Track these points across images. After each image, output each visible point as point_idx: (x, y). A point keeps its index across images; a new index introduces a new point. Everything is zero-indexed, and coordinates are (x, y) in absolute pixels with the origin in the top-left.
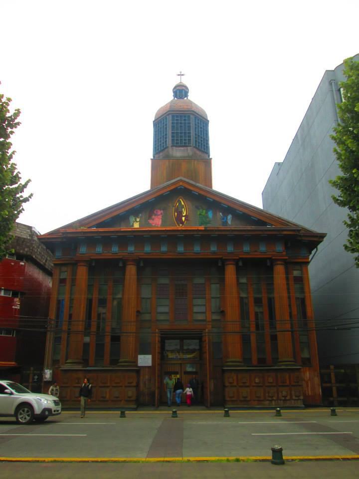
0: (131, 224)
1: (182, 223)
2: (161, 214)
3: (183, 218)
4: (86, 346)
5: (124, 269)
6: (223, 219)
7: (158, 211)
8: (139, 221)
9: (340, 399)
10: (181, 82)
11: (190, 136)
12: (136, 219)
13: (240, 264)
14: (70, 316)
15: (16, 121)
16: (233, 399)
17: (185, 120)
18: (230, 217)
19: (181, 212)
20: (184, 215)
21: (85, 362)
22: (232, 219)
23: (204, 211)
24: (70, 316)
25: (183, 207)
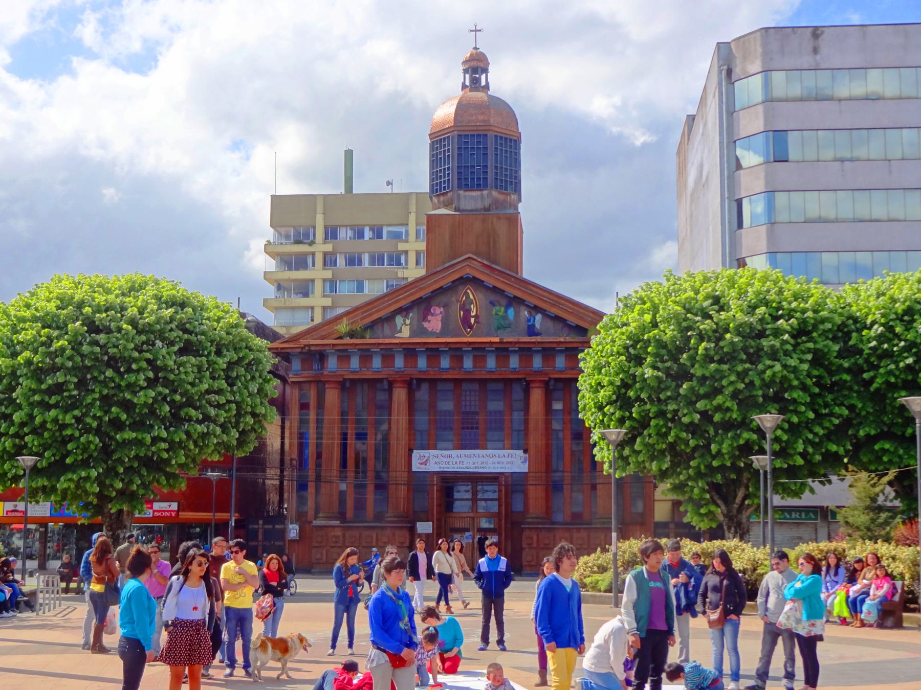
0: (399, 328)
1: (471, 327)
2: (441, 313)
3: (472, 320)
4: (342, 494)
5: (390, 390)
6: (529, 320)
7: (437, 308)
9: (823, 573)
10: (476, 48)
12: (404, 321)
14: (319, 456)
16: (532, 563)
19: (469, 311)
20: (473, 314)
21: (342, 516)
23: (503, 309)
24: (319, 456)
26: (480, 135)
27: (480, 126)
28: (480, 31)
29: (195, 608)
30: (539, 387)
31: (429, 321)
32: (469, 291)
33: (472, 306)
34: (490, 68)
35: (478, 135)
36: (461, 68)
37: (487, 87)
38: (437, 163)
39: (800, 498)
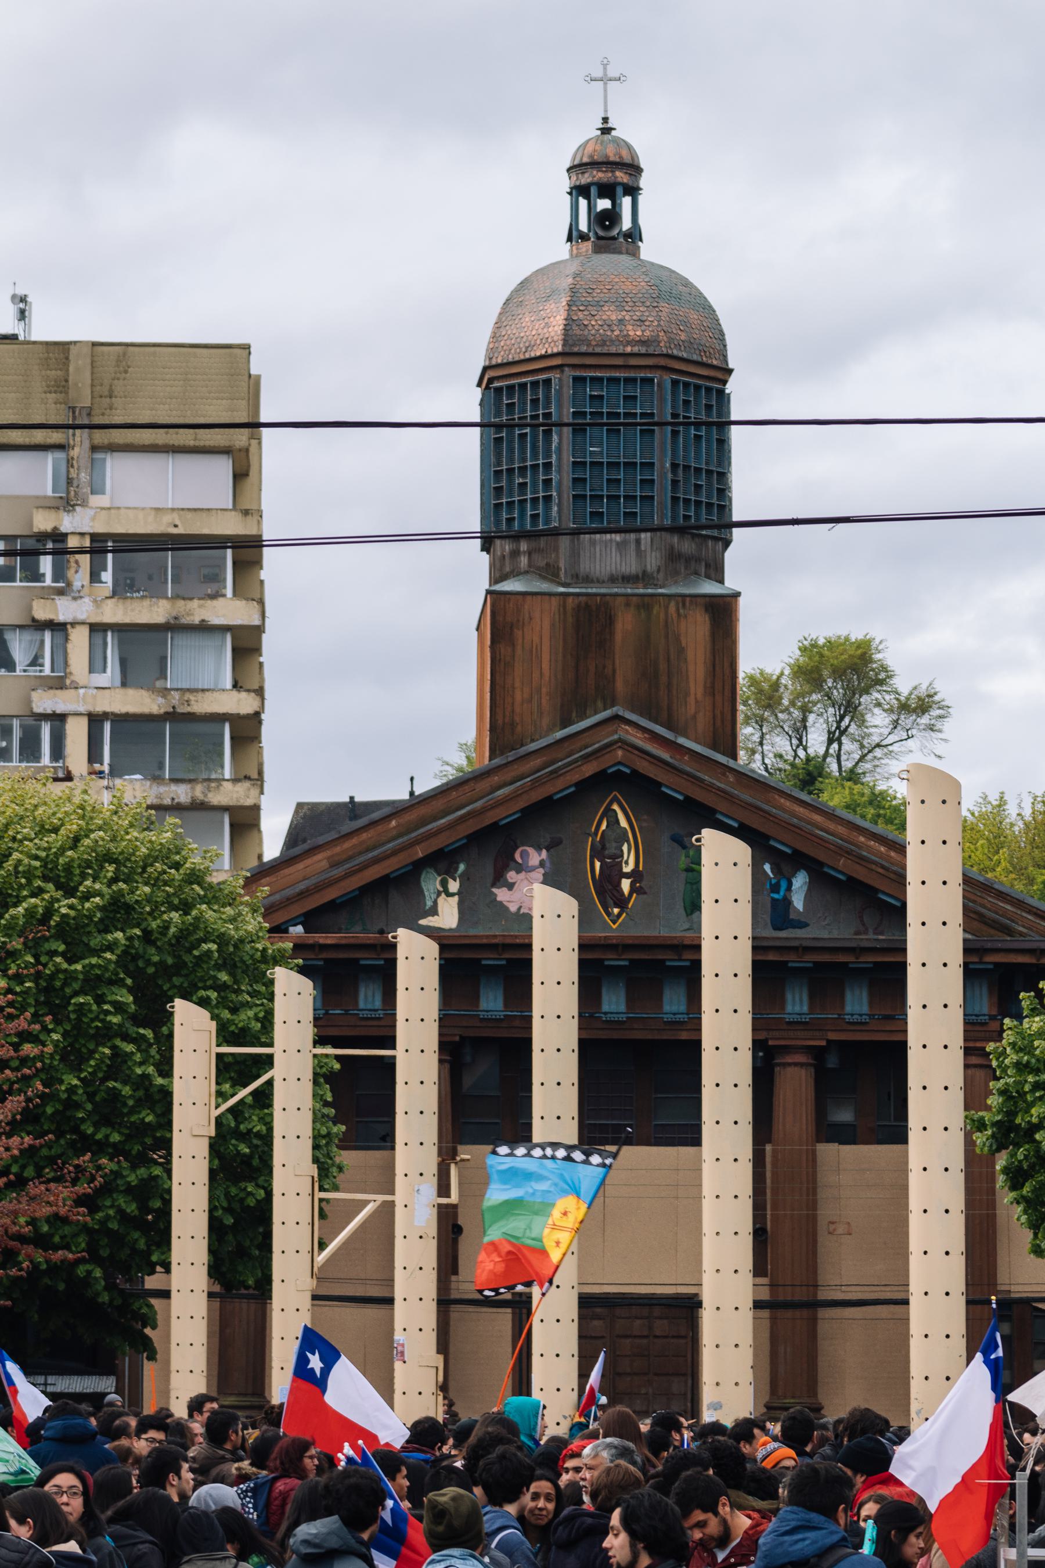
1: (622, 902)
2: (542, 864)
3: (626, 885)
7: (531, 851)
8: (459, 893)
11: (652, 465)
12: (444, 884)
13: (832, 1062)
15: (979, 1356)
17: (613, 482)
18: (800, 881)
20: (627, 869)
22: (809, 890)
25: (623, 837)
26: (634, 380)
27: (632, 355)
28: (605, 66)
29: (558, 1424)
30: (801, 1065)
31: (511, 886)
32: (615, 807)
33: (625, 848)
34: (644, 182)
35: (627, 380)
36: (565, 183)
37: (634, 235)
38: (511, 450)
39: (352, 798)
